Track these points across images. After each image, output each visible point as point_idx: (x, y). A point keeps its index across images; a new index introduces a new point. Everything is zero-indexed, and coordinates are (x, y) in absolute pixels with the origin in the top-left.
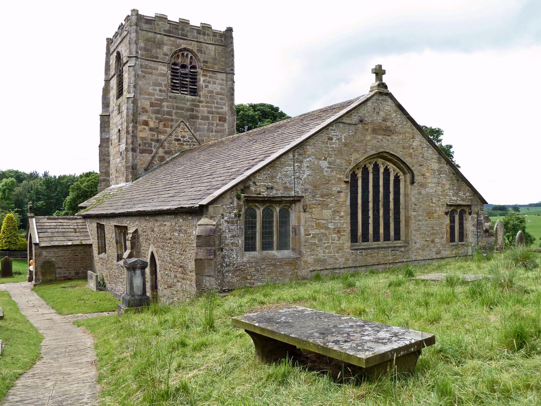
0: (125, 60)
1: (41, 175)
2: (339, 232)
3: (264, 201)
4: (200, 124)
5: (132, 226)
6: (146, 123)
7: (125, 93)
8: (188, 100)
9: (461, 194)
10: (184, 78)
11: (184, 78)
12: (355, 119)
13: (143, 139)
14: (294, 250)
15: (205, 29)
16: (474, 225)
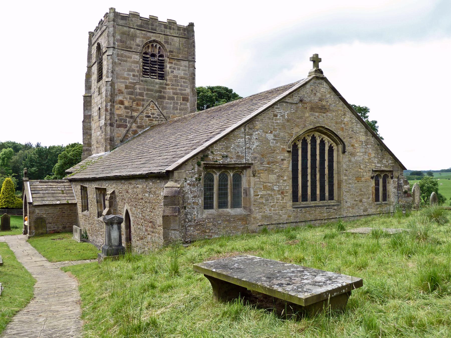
0: (104, 50)
1: (34, 145)
2: (282, 193)
3: (220, 167)
4: (167, 103)
5: (110, 188)
6: (122, 103)
7: (104, 77)
8: (157, 83)
9: (384, 161)
10: (153, 65)
11: (153, 65)
12: (296, 99)
13: (119, 115)
14: (245, 208)
15: (171, 24)
16: (395, 188)
